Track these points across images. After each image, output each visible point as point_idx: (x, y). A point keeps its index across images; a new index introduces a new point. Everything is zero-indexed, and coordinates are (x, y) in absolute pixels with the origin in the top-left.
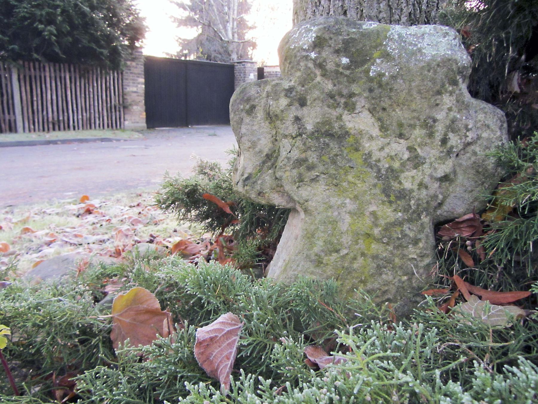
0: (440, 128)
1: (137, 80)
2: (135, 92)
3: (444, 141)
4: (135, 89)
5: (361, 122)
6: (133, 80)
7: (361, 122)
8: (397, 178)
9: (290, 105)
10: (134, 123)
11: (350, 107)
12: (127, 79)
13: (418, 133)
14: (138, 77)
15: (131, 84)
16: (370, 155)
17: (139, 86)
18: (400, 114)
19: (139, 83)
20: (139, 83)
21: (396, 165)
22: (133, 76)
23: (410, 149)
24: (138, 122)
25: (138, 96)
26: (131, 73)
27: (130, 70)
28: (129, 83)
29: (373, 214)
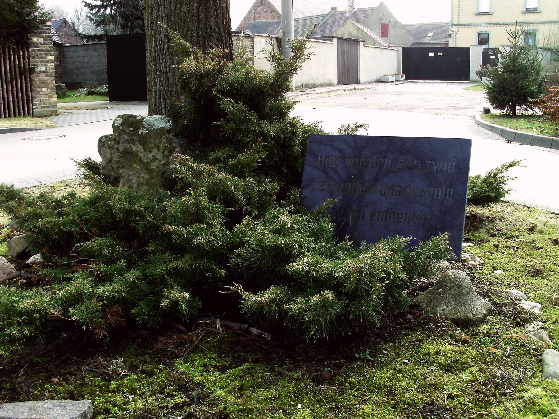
0: (161, 148)
1: (46, 58)
2: (44, 72)
3: (163, 153)
4: (43, 69)
5: (137, 148)
6: (42, 58)
7: (137, 148)
8: (149, 165)
9: (115, 144)
10: (44, 107)
11: (134, 143)
12: (34, 58)
13: (155, 150)
14: (47, 54)
15: (39, 63)
16: (141, 158)
17: (48, 65)
18: (42, 186)
19: (48, 62)
20: (48, 62)
21: (149, 161)
22: (40, 54)
23: (153, 156)
24: (48, 107)
25: (47, 76)
26: (39, 50)
27: (37, 47)
28: (37, 61)
29: (143, 177)
